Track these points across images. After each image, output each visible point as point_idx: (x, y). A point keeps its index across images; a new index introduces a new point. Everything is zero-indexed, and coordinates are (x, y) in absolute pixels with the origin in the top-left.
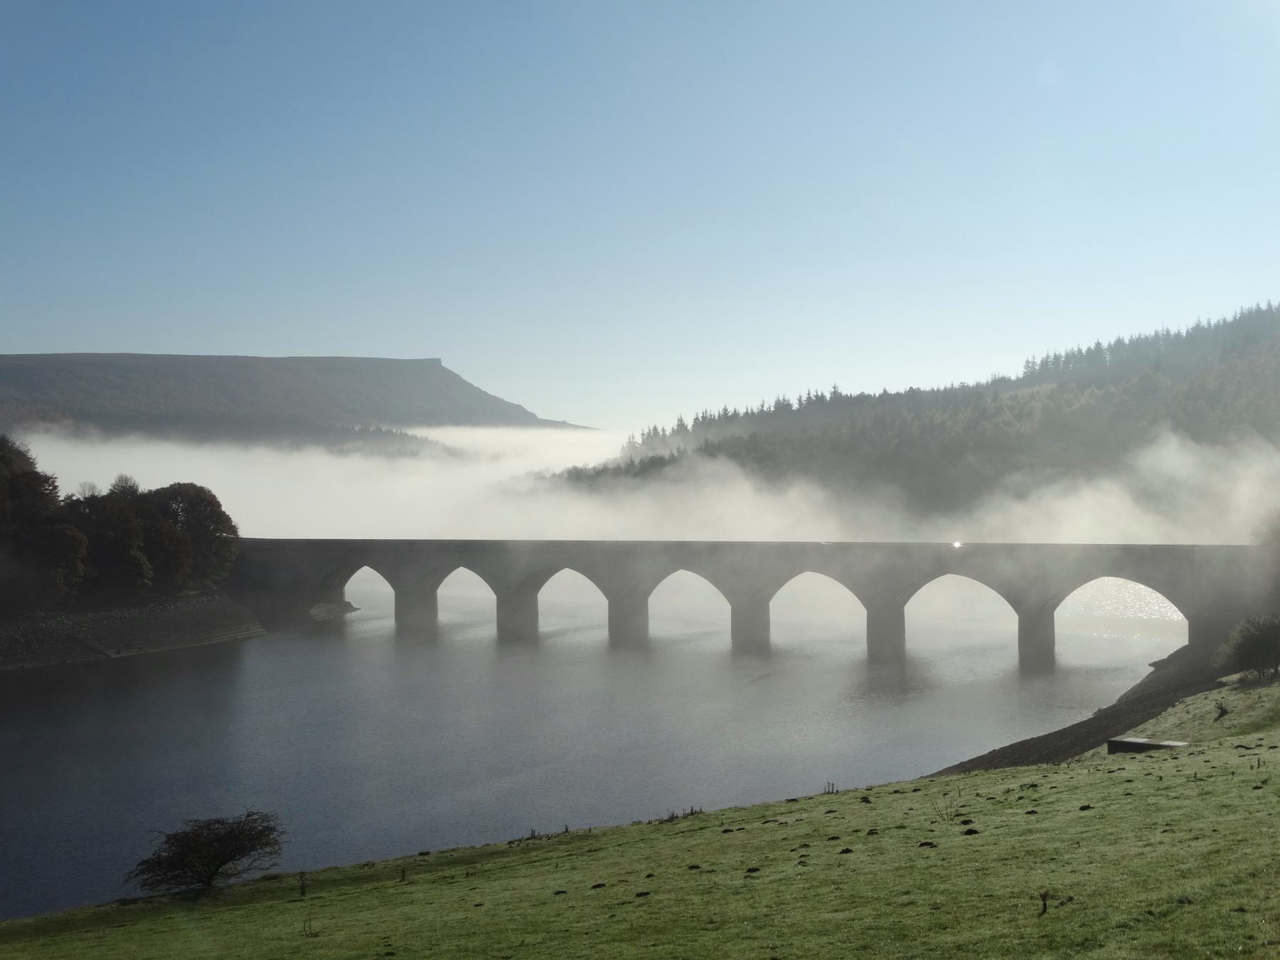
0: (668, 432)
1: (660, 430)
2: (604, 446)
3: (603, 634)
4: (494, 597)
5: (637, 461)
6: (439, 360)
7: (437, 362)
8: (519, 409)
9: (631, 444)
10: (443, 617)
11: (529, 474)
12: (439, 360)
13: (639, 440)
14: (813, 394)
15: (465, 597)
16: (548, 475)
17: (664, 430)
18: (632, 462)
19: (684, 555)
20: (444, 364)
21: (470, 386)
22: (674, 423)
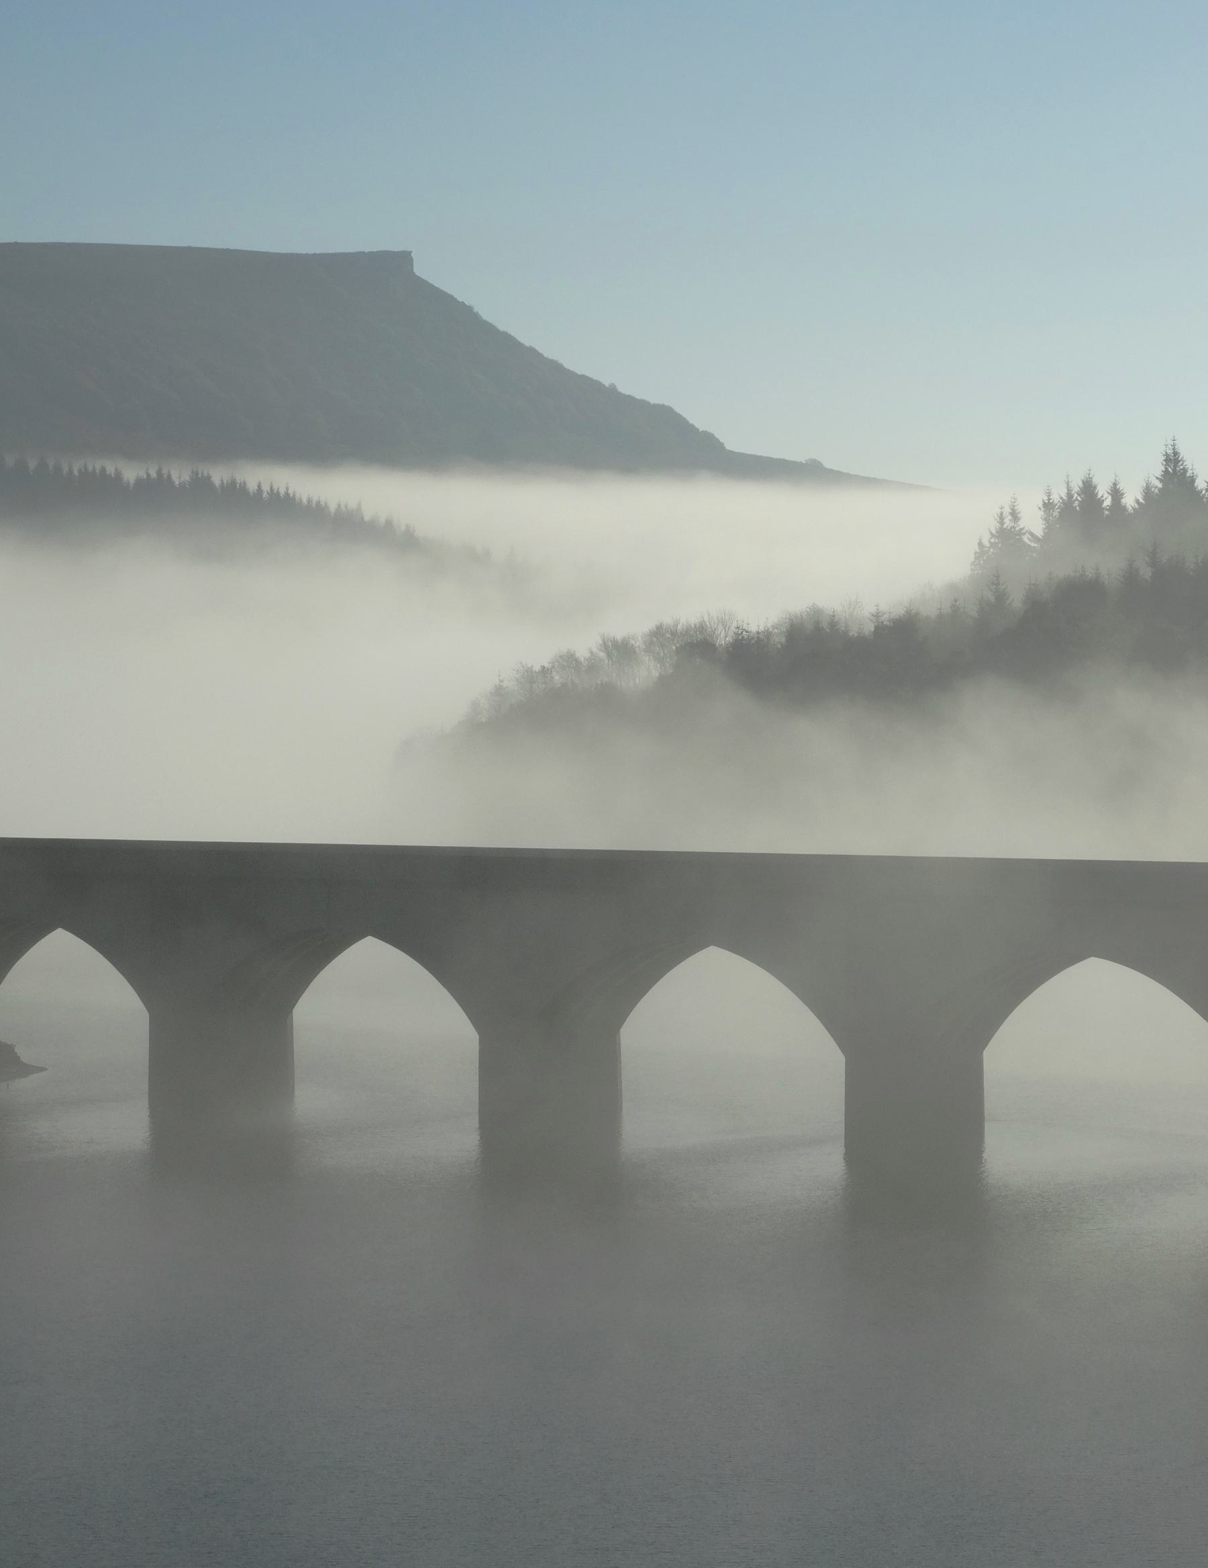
0: (1131, 499)
1: (1103, 491)
2: (899, 543)
3: (460, 1142)
4: (840, 1058)
5: (1016, 600)
6: (405, 258)
7: (396, 264)
8: (665, 417)
9: (1007, 535)
10: (311, 1100)
11: (659, 635)
12: (405, 258)
13: (1033, 522)
14: (266, 488)
15: (727, 1052)
16: (723, 639)
17: (1116, 493)
18: (1001, 597)
19: (751, 902)
20: (422, 269)
21: (508, 342)
22: (1154, 470)
